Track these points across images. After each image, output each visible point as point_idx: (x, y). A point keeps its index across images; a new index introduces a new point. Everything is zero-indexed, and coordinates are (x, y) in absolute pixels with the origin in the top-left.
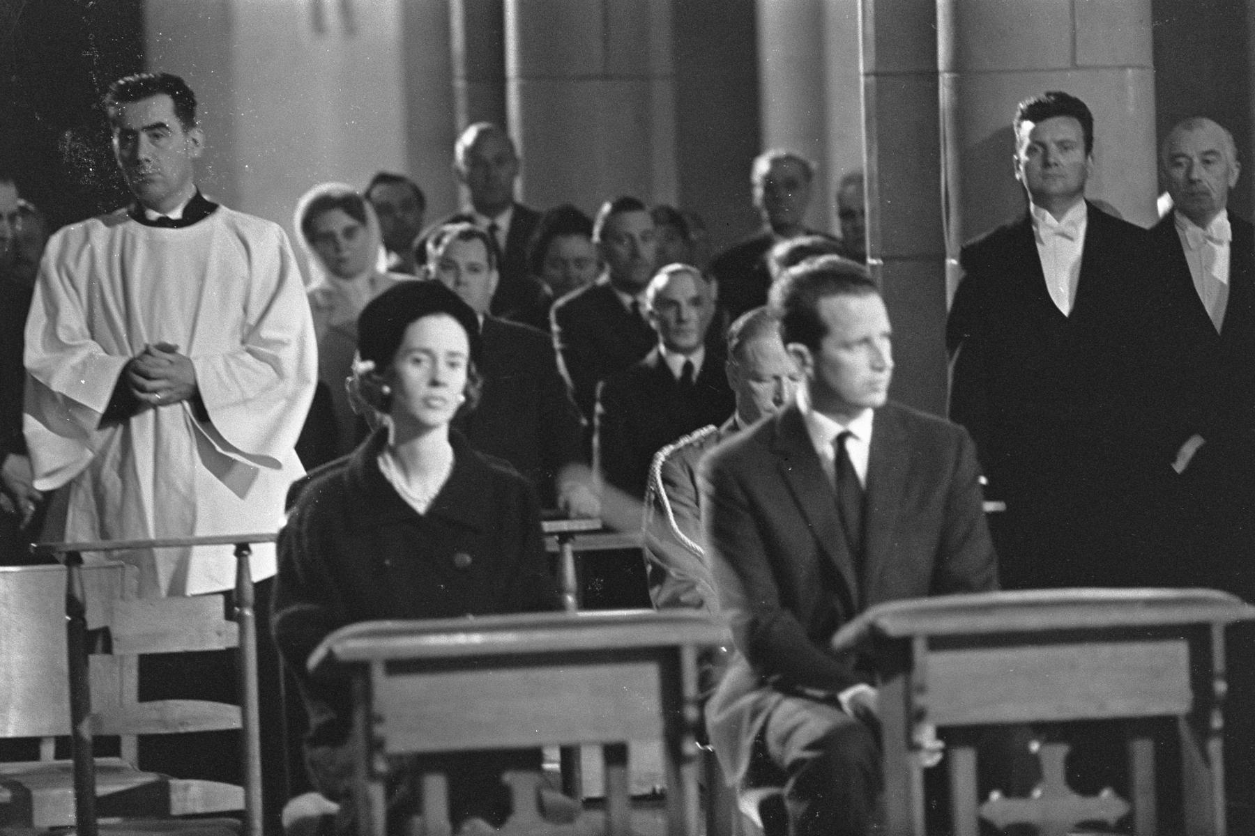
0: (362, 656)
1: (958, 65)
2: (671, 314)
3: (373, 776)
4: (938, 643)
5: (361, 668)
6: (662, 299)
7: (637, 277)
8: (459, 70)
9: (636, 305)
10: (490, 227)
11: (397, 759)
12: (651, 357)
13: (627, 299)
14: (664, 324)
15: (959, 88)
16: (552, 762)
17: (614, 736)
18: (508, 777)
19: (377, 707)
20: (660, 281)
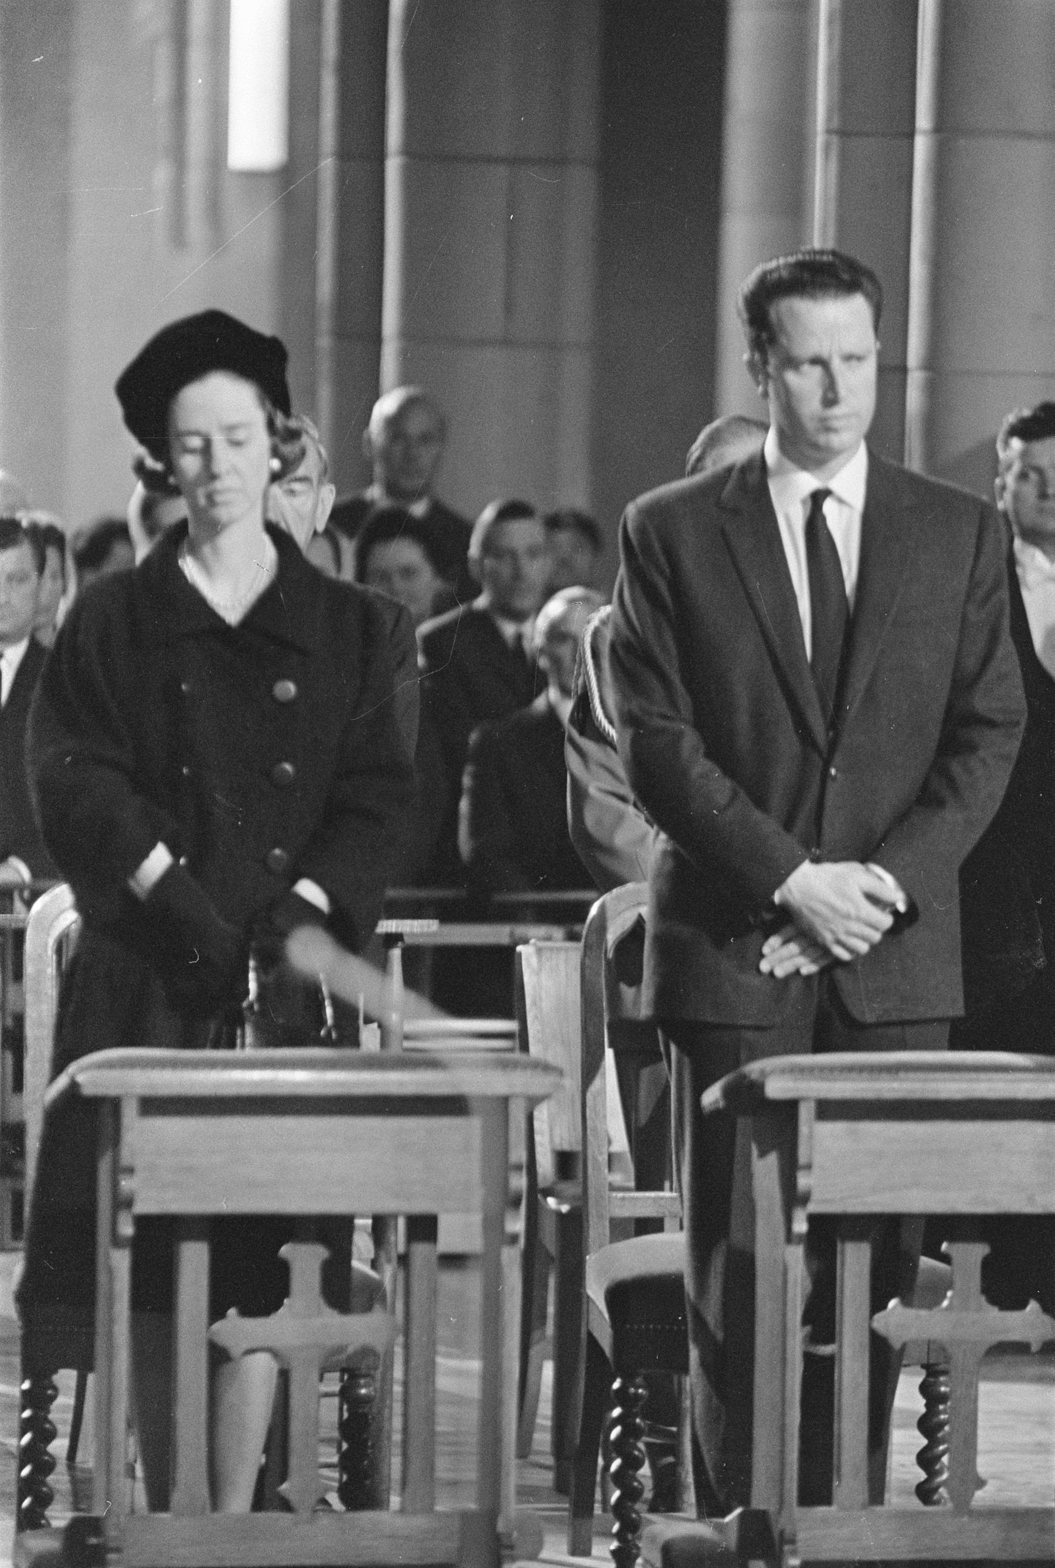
0: (112, 1092)
1: (932, 363)
2: (565, 651)
3: (117, 1241)
4: (828, 1110)
5: (113, 1105)
6: (557, 633)
7: (524, 602)
8: (325, 322)
9: (519, 637)
10: (387, 492)
11: (143, 1222)
12: (540, 704)
13: (509, 629)
14: (556, 661)
15: (933, 389)
16: (364, 1228)
17: (421, 1206)
18: (285, 1250)
19: (126, 1157)
20: (555, 608)
